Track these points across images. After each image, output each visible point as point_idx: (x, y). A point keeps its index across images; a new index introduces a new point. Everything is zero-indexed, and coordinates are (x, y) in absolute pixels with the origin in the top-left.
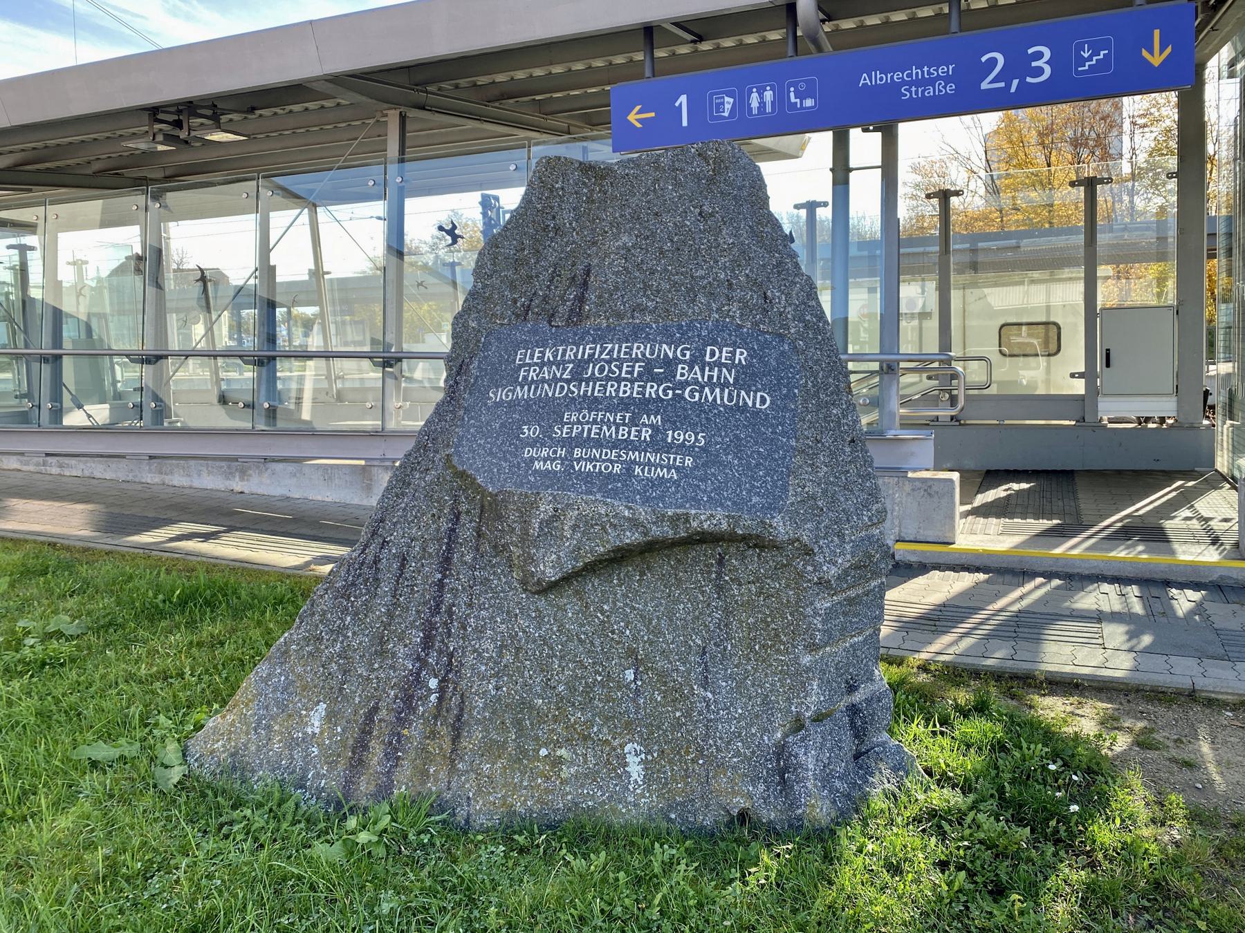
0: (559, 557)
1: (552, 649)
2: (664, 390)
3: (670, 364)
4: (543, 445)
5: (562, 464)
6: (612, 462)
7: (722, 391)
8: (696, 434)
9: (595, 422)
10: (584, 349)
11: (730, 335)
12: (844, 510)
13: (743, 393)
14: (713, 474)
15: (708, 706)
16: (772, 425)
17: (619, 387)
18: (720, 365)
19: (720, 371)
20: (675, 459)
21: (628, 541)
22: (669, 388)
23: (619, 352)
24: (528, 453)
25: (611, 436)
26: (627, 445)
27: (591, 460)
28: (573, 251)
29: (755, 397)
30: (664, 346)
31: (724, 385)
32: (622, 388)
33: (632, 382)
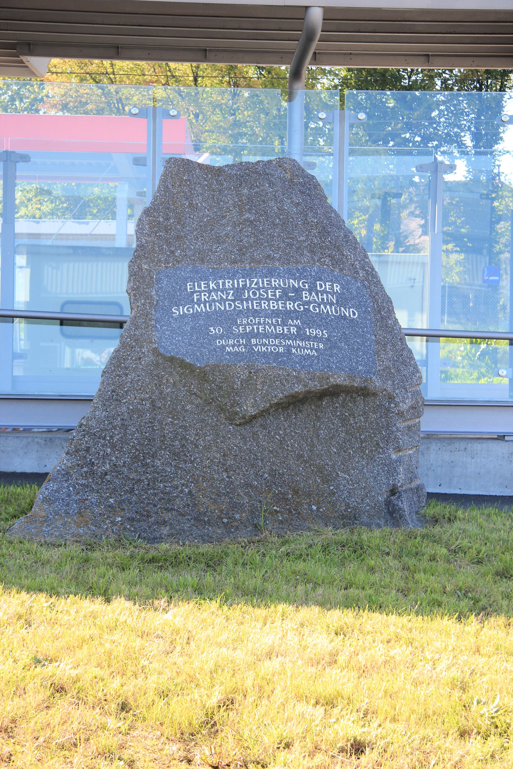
0: (256, 401)
1: (256, 455)
2: (298, 306)
3: (298, 291)
4: (229, 338)
5: (245, 348)
6: (277, 346)
7: (331, 307)
8: (322, 331)
9: (259, 323)
10: (238, 282)
11: (329, 276)
12: (404, 375)
13: (342, 309)
14: (336, 354)
15: (348, 482)
16: (361, 328)
17: (269, 304)
18: (325, 292)
19: (327, 296)
20: (313, 345)
21: (296, 390)
22: (300, 305)
23: (263, 283)
24: (219, 343)
25: (328, 312)
26: (283, 336)
27: (265, 345)
28: (208, 221)
29: (349, 311)
30: (291, 280)
31: (331, 304)
32: (271, 305)
33: (277, 301)
